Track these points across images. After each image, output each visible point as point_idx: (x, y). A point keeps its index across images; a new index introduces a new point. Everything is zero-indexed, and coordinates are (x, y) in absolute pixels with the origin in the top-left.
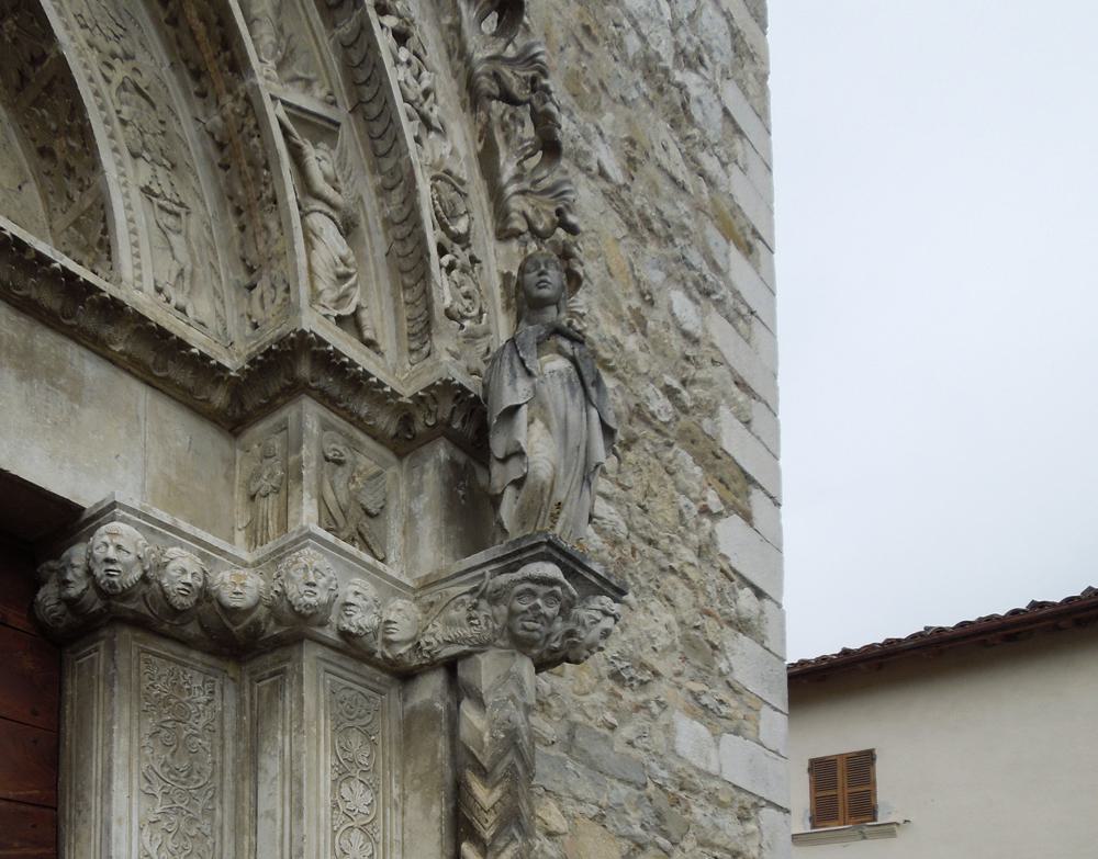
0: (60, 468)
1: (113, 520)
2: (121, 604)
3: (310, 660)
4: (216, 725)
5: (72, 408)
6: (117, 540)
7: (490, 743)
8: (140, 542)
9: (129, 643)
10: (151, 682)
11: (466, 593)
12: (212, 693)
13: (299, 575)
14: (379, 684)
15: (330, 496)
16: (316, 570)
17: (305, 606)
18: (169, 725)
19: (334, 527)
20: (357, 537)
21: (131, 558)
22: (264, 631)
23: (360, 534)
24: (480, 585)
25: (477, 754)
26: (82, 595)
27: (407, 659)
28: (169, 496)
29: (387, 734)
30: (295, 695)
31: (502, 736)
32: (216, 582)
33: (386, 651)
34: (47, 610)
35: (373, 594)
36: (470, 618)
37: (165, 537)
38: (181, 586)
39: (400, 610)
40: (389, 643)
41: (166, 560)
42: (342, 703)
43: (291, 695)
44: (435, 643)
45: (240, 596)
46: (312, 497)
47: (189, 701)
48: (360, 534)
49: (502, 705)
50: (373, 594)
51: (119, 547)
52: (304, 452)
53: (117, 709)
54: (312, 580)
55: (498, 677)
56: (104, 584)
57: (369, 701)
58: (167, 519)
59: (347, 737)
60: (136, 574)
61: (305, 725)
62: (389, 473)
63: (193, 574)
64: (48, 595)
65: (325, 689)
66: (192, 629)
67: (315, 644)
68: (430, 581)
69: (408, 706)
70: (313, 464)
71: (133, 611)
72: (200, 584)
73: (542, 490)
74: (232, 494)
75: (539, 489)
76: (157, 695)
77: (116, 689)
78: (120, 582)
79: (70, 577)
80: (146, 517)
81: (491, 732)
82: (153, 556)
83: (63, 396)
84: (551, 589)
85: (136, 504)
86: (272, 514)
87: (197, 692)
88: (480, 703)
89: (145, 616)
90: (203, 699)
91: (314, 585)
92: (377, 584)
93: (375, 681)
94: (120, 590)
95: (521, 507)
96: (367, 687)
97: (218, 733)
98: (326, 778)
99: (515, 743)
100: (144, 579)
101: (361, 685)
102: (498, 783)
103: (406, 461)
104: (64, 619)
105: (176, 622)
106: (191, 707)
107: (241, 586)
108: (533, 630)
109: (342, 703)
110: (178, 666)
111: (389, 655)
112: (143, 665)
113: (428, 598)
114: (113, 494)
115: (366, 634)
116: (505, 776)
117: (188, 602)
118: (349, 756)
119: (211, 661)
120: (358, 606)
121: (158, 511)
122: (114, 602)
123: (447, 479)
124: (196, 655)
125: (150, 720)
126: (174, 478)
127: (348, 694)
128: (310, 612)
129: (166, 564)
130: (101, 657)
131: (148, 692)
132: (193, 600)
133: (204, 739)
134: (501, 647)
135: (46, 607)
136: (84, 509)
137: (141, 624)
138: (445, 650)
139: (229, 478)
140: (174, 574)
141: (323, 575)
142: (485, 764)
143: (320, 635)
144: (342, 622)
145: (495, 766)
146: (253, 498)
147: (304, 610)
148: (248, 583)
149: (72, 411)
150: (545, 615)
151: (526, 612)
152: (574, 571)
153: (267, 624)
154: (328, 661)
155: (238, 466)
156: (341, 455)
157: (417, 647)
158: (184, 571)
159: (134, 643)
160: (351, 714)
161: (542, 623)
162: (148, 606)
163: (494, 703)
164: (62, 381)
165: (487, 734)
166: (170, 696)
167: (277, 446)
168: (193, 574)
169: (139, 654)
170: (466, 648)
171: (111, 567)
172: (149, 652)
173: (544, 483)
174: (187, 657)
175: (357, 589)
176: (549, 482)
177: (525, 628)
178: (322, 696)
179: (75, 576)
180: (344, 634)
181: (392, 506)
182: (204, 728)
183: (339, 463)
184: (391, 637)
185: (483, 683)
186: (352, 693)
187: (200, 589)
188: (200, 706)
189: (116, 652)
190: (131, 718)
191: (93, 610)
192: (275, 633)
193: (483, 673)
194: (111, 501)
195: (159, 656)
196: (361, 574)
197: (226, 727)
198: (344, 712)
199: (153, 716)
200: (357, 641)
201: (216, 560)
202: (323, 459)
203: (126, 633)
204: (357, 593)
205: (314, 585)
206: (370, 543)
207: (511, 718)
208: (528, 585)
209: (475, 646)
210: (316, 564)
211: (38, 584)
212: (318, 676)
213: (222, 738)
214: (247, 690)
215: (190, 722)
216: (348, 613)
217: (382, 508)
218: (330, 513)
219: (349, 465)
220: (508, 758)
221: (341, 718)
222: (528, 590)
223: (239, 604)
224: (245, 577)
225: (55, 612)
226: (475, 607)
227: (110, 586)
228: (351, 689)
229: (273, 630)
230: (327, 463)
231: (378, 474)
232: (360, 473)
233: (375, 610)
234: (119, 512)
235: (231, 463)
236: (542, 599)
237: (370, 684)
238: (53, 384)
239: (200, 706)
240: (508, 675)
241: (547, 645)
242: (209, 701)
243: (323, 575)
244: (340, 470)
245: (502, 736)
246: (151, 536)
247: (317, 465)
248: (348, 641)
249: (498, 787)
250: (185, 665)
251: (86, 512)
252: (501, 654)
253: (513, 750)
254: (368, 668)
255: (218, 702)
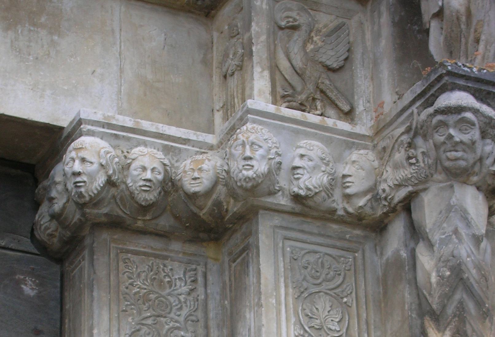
0: (42, 97)
1: (81, 135)
2: (95, 211)
3: (266, 233)
4: (200, 314)
5: (52, 40)
6: (82, 154)
7: (438, 283)
8: (103, 151)
9: (105, 244)
10: (130, 281)
11: (402, 134)
12: (194, 281)
13: (238, 152)
14: (349, 241)
15: (284, 64)
16: (253, 143)
17: (245, 179)
18: (149, 321)
19: (290, 92)
20: (318, 96)
21: (95, 166)
22: (227, 211)
23: (322, 92)
24: (411, 123)
25: (428, 297)
26: (64, 208)
27: (368, 210)
28: (145, 95)
29: (362, 294)
30: (255, 269)
31: (448, 273)
32: (180, 171)
33: (347, 206)
34: (43, 227)
35: (319, 153)
36: (409, 158)
37: (129, 139)
38: (142, 183)
39: (354, 162)
40: (348, 197)
41: (129, 161)
42: (306, 268)
43: (253, 268)
44: (387, 189)
45: (198, 181)
46: (263, 70)
47: (169, 294)
48: (322, 92)
49: (445, 242)
50: (319, 153)
51: (83, 160)
52: (254, 27)
53: (96, 312)
54: (248, 153)
55: (441, 212)
56: (74, 195)
57: (338, 262)
58: (129, 122)
59: (313, 303)
60: (101, 180)
61: (263, 297)
62: (353, 23)
63: (153, 170)
64: (43, 217)
65: (284, 256)
66: (165, 222)
67: (272, 213)
68: (381, 126)
69: (385, 258)
70: (263, 38)
71: (106, 215)
72: (160, 177)
73: (458, 19)
74: (211, 77)
75: (455, 19)
76: (135, 294)
77: (95, 294)
78: (87, 191)
79: (54, 194)
80: (110, 126)
81: (438, 271)
82: (117, 160)
83: (43, 33)
84: (460, 117)
85: (99, 117)
86: (237, 91)
87: (178, 283)
88: (431, 246)
89: (118, 216)
90: (185, 289)
91: (251, 158)
92: (328, 142)
93: (346, 240)
94: (87, 198)
95: (446, 38)
96: (334, 247)
97: (201, 323)
98: (373, 333)
99: (462, 279)
100: (110, 183)
101: (328, 246)
102: (449, 324)
103: (369, 7)
104: (57, 234)
105: (148, 218)
106: (172, 299)
107: (199, 172)
108: (457, 159)
109: (306, 268)
110: (158, 261)
111: (350, 210)
112: (122, 265)
113: (382, 144)
114: (79, 114)
115: (316, 193)
116: (455, 316)
117: (151, 197)
118: (316, 323)
119: (192, 248)
120: (304, 168)
121: (120, 117)
122: (88, 211)
123: (397, 19)
124: (176, 246)
125: (130, 319)
126: (150, 77)
127: (312, 258)
128: (250, 184)
129: (129, 165)
130: (86, 264)
131: (127, 291)
132: (156, 193)
133: (187, 331)
134: (441, 182)
135: (41, 225)
136: (61, 129)
137: (115, 224)
138: (398, 194)
139: (206, 62)
140: (135, 173)
141: (260, 147)
142: (434, 306)
143: (272, 203)
144: (292, 187)
145: (444, 307)
146: (225, 77)
147: (244, 184)
148: (205, 166)
149: (53, 44)
150: (461, 142)
151: (444, 143)
152: (489, 93)
153: (228, 203)
154: (286, 228)
155: (215, 48)
156: (295, 20)
157: (376, 198)
158: (144, 169)
159: (113, 245)
160: (318, 278)
161: (464, 151)
162: (118, 206)
163: (441, 240)
164: (43, 19)
165: (434, 274)
166: (150, 292)
167: (239, 25)
168: (153, 170)
169: (117, 255)
170: (410, 189)
171: (79, 179)
172: (128, 251)
173: (458, 12)
174: (166, 250)
175: (302, 151)
176: (463, 10)
177: (449, 159)
178: (281, 265)
179: (57, 191)
180: (296, 198)
181: (358, 55)
182: (186, 320)
183: (294, 28)
184: (348, 191)
185: (427, 221)
186: (317, 256)
187: (164, 180)
188: (182, 298)
189: (95, 257)
190: (110, 319)
191: (74, 221)
192: (235, 210)
193: (427, 211)
194: (77, 119)
195: (136, 253)
196: (308, 135)
197: (211, 315)
198: (308, 278)
199: (133, 314)
200: (310, 203)
201: (180, 149)
202: (276, 29)
203: (105, 235)
204: (302, 156)
205: (251, 158)
206: (334, 98)
207: (455, 252)
208: (439, 117)
209: (416, 185)
210: (252, 138)
211: (37, 205)
212: (276, 245)
213: (207, 327)
214: (227, 273)
215: (172, 315)
216: (296, 176)
217: (346, 59)
218: (286, 80)
219: (304, 28)
220: (457, 296)
221: (305, 284)
222: (441, 121)
223: (197, 189)
224: (202, 161)
225: (49, 228)
226: (410, 145)
227: (79, 197)
228: (316, 252)
229: (234, 207)
230: (280, 33)
231: (338, 28)
232: (319, 31)
233: (323, 169)
234: (85, 127)
235: (207, 47)
236: (455, 127)
237: (338, 244)
238: (34, 25)
239: (182, 298)
240: (450, 208)
241: (484, 170)
242: (192, 290)
243: (260, 147)
244: (296, 35)
245: (448, 273)
246: (117, 142)
247: (268, 37)
248: (303, 204)
249: (448, 329)
250: (165, 258)
251: (65, 129)
252: (442, 189)
253: (461, 288)
254: (335, 226)
255: (201, 290)
